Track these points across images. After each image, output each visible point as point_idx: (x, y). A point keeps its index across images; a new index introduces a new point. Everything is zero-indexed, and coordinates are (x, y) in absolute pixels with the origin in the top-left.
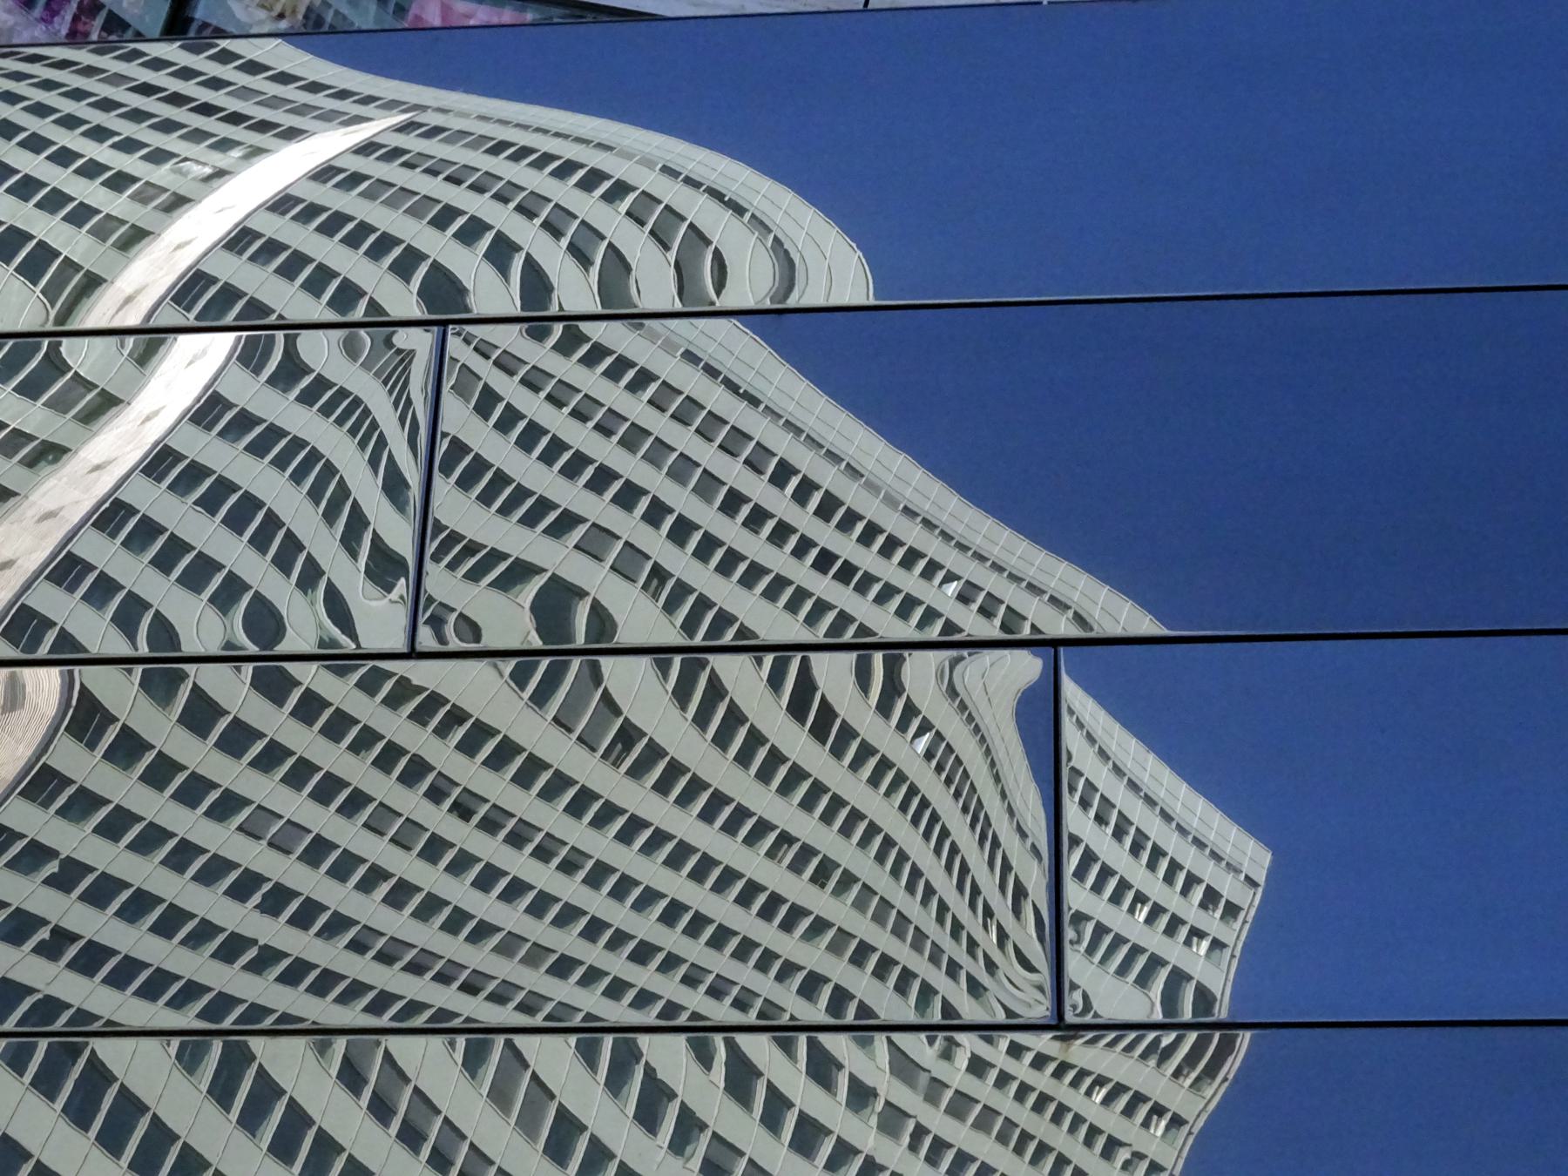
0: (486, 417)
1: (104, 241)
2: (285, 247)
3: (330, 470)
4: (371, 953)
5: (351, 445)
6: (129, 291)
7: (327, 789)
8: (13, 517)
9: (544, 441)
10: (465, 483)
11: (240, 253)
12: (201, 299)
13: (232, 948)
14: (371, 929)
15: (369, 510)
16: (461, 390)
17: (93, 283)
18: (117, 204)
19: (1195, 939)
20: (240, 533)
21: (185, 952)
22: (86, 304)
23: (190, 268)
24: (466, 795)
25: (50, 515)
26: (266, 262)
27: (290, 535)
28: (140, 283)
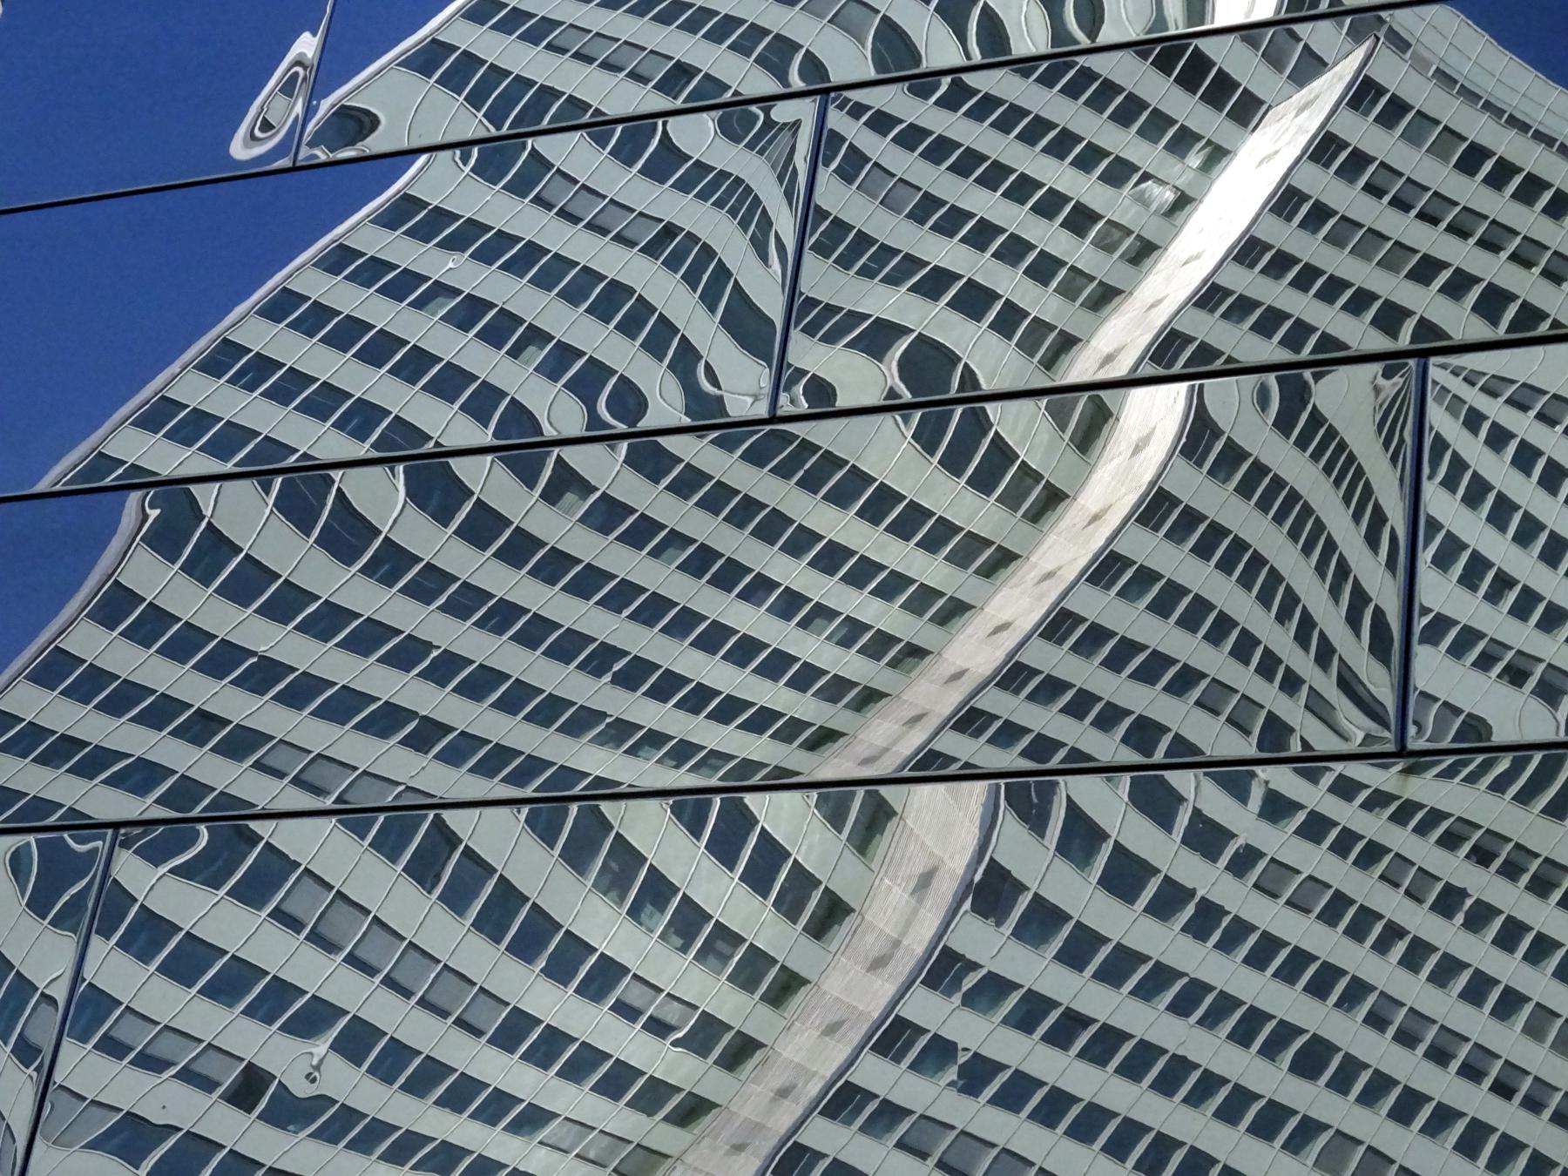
0: (1453, 491)
1: (1074, 300)
2: (1257, 304)
3: (1307, 510)
4: (1444, 225)
5: (1326, 484)
6: (1107, 350)
7: (983, 234)
8: (1014, 581)
9: (1378, 928)
10: (1450, 484)
11: (1212, 311)
12: (1172, 356)
13: (976, 1074)
14: (1532, 388)
15: (1352, 561)
16: (1439, 400)
17: (1068, 342)
18: (1078, 252)
19: (649, 908)
20: (1345, 857)
21: (1136, 1005)
22: (1065, 360)
23: (1164, 327)
24: (1459, 824)
25: (1049, 575)
26: (1241, 320)
27: (1273, 570)
28: (1118, 340)
